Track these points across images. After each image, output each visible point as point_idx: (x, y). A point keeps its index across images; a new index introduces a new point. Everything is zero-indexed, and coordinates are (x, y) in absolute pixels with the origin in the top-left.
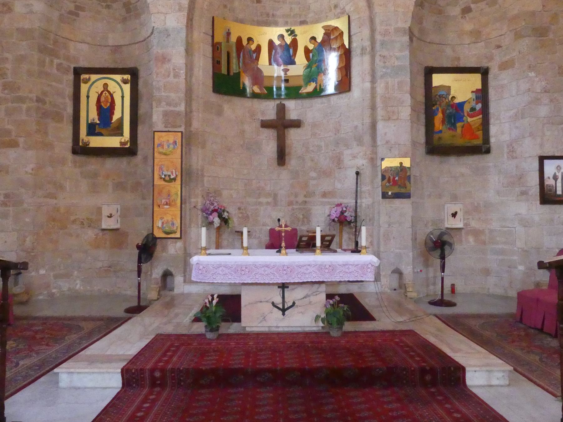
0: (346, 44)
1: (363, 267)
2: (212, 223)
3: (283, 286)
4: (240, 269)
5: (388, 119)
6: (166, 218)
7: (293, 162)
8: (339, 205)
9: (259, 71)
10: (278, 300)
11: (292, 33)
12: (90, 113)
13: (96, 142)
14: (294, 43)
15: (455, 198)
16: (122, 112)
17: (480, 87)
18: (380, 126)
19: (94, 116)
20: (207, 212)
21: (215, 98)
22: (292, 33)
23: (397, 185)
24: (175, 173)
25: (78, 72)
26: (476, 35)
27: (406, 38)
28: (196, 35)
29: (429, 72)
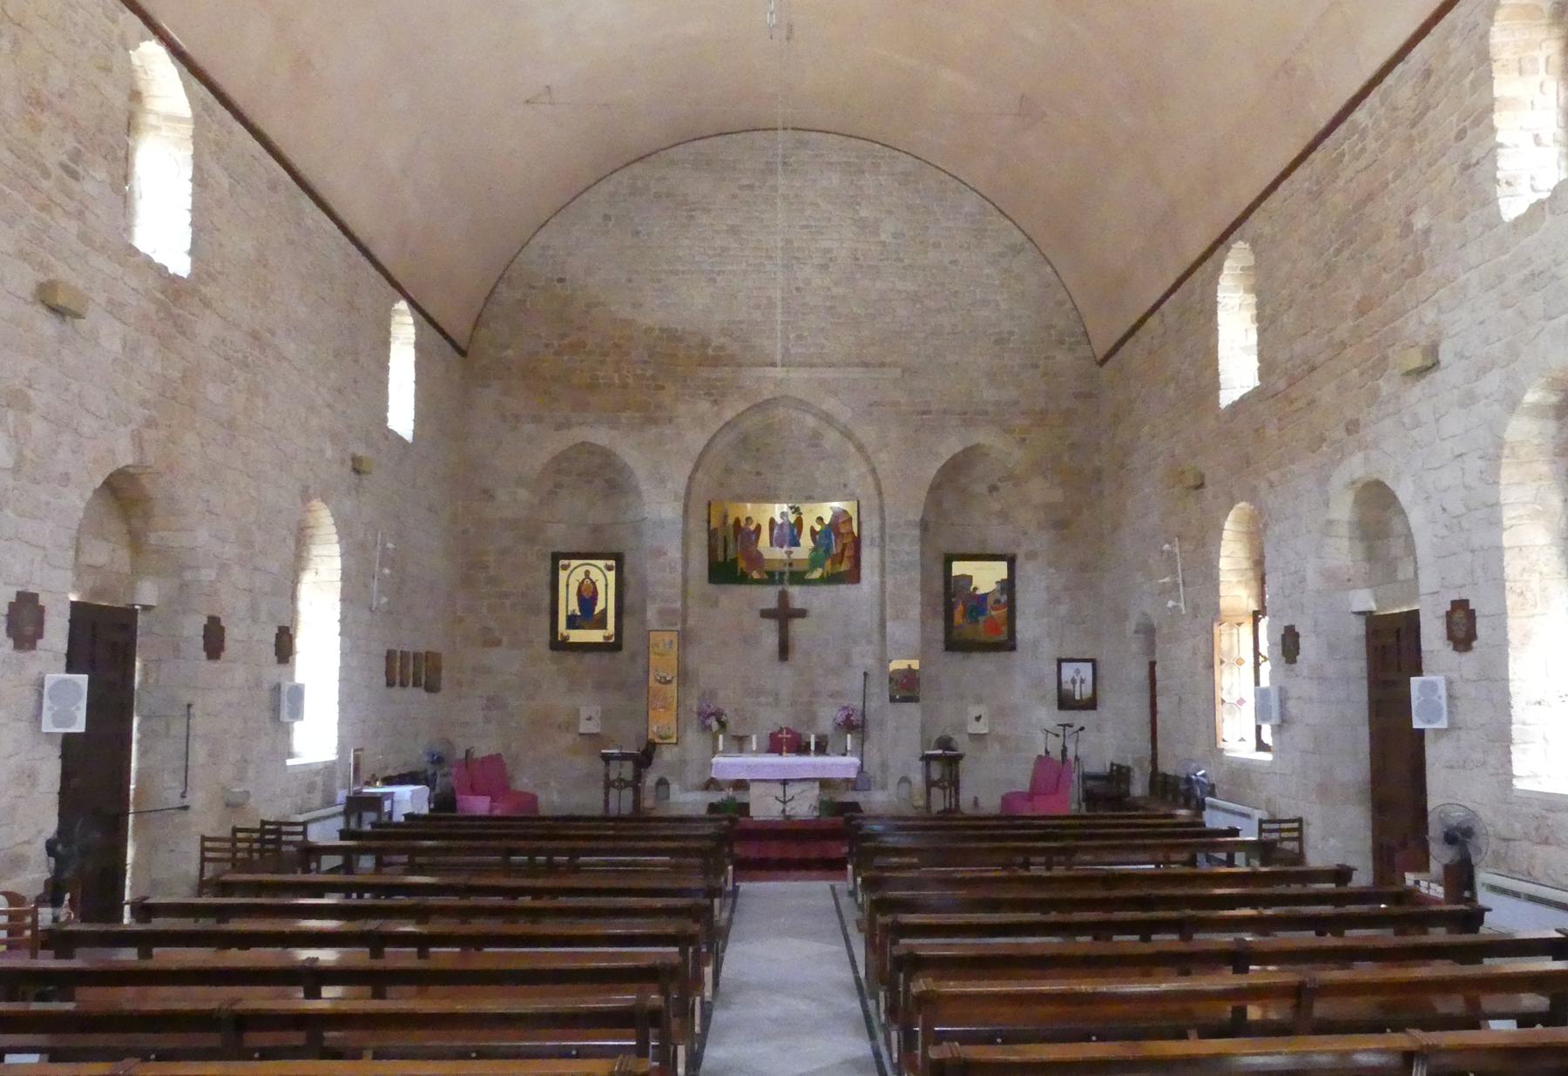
0: (855, 530)
1: (847, 766)
2: (710, 727)
3: (785, 782)
4: (749, 767)
5: (897, 618)
6: (661, 723)
7: (796, 656)
8: (845, 708)
9: (760, 555)
10: (780, 794)
11: (796, 510)
12: (569, 603)
13: (577, 636)
14: (799, 522)
15: (979, 700)
16: (606, 601)
17: (1005, 576)
18: (889, 624)
19: (574, 606)
20: (704, 715)
21: (712, 588)
22: (796, 510)
23: (906, 688)
24: (671, 674)
25: (556, 557)
26: (1004, 516)
27: (917, 532)
28: (692, 525)
29: (949, 560)
